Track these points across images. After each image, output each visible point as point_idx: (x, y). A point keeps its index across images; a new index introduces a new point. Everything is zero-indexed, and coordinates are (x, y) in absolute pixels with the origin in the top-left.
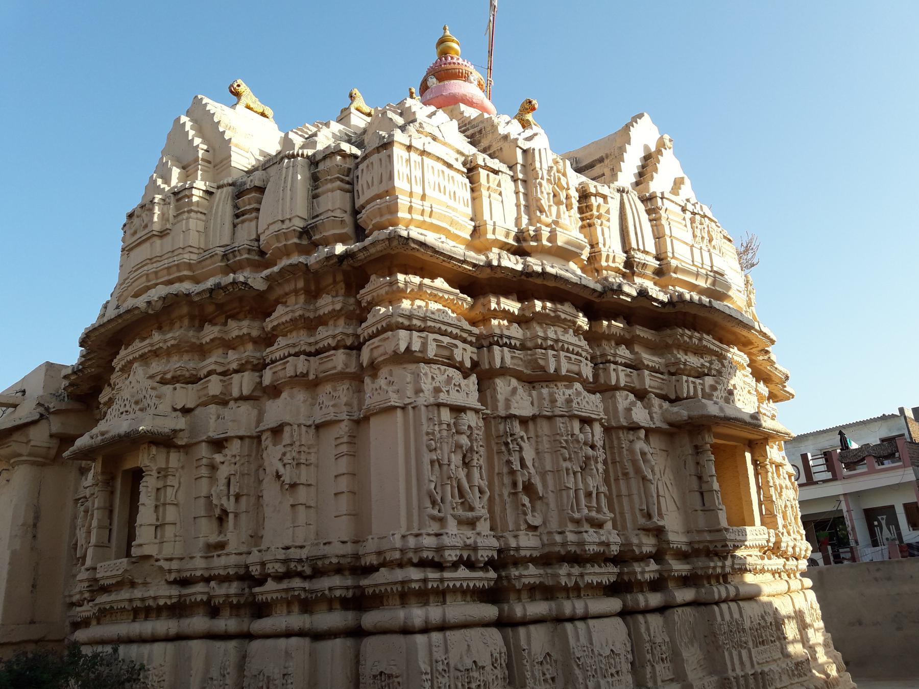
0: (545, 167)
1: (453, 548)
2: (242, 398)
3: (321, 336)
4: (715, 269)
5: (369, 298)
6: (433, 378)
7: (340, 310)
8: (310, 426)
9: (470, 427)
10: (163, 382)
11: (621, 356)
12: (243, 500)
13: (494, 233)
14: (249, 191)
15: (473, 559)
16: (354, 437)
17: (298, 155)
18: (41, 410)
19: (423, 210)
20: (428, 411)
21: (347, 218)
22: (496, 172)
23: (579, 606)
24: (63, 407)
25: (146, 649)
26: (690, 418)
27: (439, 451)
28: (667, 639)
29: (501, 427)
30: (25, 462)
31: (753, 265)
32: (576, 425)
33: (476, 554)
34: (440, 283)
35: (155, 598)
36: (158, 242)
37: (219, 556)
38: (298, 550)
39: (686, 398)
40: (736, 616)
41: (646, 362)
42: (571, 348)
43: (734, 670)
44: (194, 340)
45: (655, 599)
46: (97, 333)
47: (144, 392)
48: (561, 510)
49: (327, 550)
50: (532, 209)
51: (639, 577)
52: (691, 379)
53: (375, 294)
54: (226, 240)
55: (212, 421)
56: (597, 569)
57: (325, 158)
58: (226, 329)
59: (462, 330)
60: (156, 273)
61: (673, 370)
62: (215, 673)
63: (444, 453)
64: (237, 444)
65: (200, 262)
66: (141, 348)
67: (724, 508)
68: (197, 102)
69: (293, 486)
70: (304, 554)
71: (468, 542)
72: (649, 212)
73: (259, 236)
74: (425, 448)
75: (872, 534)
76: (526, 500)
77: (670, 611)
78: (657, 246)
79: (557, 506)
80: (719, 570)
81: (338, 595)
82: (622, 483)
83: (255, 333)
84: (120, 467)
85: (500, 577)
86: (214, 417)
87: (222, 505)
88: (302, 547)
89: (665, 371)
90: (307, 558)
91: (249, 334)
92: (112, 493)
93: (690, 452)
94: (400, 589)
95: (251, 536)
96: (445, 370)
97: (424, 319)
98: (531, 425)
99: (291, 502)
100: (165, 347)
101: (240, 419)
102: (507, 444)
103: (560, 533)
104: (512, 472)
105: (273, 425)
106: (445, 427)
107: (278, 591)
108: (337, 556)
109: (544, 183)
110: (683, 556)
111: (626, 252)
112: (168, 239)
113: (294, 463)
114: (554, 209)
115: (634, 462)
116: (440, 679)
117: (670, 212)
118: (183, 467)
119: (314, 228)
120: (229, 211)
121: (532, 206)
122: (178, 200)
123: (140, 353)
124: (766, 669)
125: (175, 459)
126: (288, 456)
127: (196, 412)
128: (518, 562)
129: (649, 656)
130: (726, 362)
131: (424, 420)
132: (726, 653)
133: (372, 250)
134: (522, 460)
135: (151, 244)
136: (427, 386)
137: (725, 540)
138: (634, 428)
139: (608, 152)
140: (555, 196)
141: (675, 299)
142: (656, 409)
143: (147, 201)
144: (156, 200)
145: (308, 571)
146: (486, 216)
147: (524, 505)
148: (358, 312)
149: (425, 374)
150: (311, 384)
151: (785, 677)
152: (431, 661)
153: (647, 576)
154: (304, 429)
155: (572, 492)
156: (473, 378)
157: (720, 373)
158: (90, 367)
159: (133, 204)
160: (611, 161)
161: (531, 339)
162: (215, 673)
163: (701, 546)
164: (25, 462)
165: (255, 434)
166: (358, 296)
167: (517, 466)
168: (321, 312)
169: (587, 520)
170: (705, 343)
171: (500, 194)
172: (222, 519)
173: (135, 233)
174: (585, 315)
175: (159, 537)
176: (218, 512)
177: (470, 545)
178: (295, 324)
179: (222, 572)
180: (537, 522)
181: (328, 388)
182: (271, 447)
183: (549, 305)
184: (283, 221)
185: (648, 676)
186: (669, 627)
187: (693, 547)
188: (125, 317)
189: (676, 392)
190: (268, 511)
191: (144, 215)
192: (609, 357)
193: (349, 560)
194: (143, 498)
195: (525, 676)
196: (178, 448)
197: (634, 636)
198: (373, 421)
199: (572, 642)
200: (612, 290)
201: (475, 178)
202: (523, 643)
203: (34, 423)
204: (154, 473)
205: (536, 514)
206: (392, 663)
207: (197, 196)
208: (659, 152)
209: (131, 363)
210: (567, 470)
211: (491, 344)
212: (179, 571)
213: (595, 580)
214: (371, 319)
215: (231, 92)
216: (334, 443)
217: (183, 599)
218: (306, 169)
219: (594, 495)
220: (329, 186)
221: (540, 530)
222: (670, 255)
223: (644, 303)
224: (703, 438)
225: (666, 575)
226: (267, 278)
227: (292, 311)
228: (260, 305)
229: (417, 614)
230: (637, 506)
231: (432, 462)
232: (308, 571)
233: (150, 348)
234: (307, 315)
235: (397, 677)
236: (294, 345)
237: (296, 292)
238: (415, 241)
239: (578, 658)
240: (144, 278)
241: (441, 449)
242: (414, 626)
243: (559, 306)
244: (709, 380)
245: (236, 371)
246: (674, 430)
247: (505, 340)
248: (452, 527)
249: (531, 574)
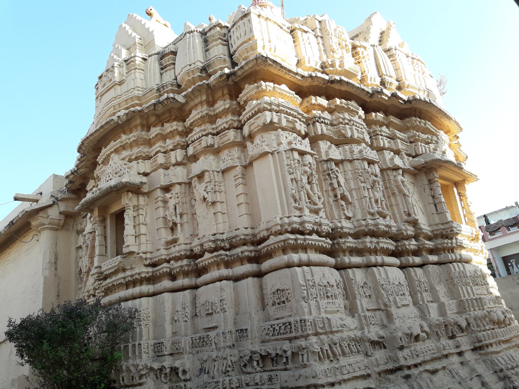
0: (333, 30)
1: (309, 222)
2: (178, 164)
3: (219, 124)
4: (428, 88)
5: (245, 98)
6: (286, 137)
7: (228, 108)
8: (218, 172)
9: (310, 163)
10: (130, 161)
11: (384, 132)
12: (185, 216)
13: (309, 63)
14: (167, 54)
15: (320, 230)
16: (244, 175)
17: (194, 31)
18: (53, 199)
19: (271, 48)
20: (286, 154)
21: (227, 58)
22: (306, 32)
23: (379, 259)
24: (66, 196)
25: (137, 301)
26: (426, 163)
27: (295, 174)
28: (427, 281)
29: (325, 166)
30: (47, 228)
31: (444, 93)
32: (366, 164)
33: (321, 228)
34: (284, 87)
35: (139, 274)
36: (118, 87)
37: (174, 247)
38: (221, 235)
39: (421, 155)
40: (462, 269)
41: (398, 135)
42: (358, 125)
43: (464, 296)
44: (145, 137)
45: (417, 260)
46: (88, 140)
47: (120, 167)
48: (362, 209)
49: (237, 233)
50: (328, 51)
51: (408, 247)
52: (423, 144)
53: (248, 95)
54: (158, 81)
55: (162, 177)
56: (385, 240)
57: (210, 29)
58: (163, 128)
59: (299, 114)
60: (119, 104)
61: (412, 140)
62: (179, 308)
63: (298, 175)
64: (178, 187)
65: (144, 95)
66: (115, 145)
67: (449, 211)
68: (130, 17)
69: (214, 203)
70: (224, 237)
71: (317, 220)
72: (390, 57)
73: (176, 77)
74: (287, 173)
75: (508, 270)
76: (343, 203)
77: (426, 266)
78: (397, 74)
79: (360, 207)
80: (450, 245)
81: (247, 255)
82: (392, 199)
83: (180, 129)
84: (110, 208)
85: (333, 244)
86: (163, 175)
87: (173, 220)
88: (222, 234)
89: (408, 141)
90: (226, 239)
91: (177, 129)
92: (105, 227)
93: (427, 183)
94: (283, 244)
95: (191, 235)
96: (292, 134)
97: (278, 105)
98: (340, 165)
99: (214, 211)
100: (129, 142)
101: (178, 174)
102: (329, 175)
103: (364, 220)
104: (334, 189)
105: (198, 172)
106: (296, 161)
107: (212, 257)
108: (244, 235)
109: (333, 37)
110: (430, 239)
111: (380, 77)
112: (124, 85)
113: (213, 191)
114: (340, 51)
115: (398, 187)
116: (311, 290)
117: (400, 58)
118: (147, 205)
119: (209, 66)
120: (157, 67)
121: (327, 50)
122: (127, 65)
123: (114, 148)
124: (482, 297)
125: (142, 200)
126: (209, 187)
127: (152, 174)
128: (343, 235)
129: (418, 288)
130: (439, 137)
131: (285, 158)
132: (459, 288)
133: (246, 68)
134: (338, 182)
135: (115, 90)
136: (284, 141)
137: (452, 227)
138: (396, 169)
139: (361, 31)
140: (339, 44)
141: (411, 98)
142: (406, 160)
143: (110, 67)
144: (115, 65)
145: (228, 246)
146: (304, 54)
147: (342, 206)
148: (238, 109)
149: (282, 135)
150: (216, 151)
151: (491, 303)
152: (305, 280)
153: (412, 247)
154: (216, 173)
155: (368, 199)
156: (307, 140)
157: (437, 142)
158: (82, 167)
159: (102, 70)
160: (363, 35)
161: (336, 120)
162: (179, 308)
163: (438, 232)
164: (47, 228)
165: (187, 181)
166: (238, 99)
167: (336, 185)
168: (218, 111)
169: (377, 213)
170: (427, 126)
171: (309, 43)
172: (173, 228)
173: (104, 85)
174: (363, 110)
175: (137, 242)
176: (171, 224)
177: (317, 223)
178: (203, 120)
179: (177, 254)
180: (350, 215)
181: (226, 152)
182: (198, 185)
183: (343, 101)
184: (190, 65)
185: (420, 299)
186: (427, 274)
187: (434, 234)
188: (105, 128)
189: (415, 152)
190: (199, 220)
191: (109, 75)
192: (378, 132)
193: (250, 237)
194: (126, 221)
195: (355, 294)
196: (143, 194)
197: (409, 279)
198: (255, 164)
199: (378, 277)
200: (378, 92)
201: (295, 35)
202: (351, 276)
203: (50, 206)
204: (131, 208)
205: (349, 211)
206: (284, 283)
207: (138, 60)
208: (389, 29)
209: (109, 156)
210: (364, 187)
211: (314, 122)
212: (151, 259)
213: (385, 246)
214: (248, 108)
215: (147, 13)
216: (233, 179)
217: (155, 274)
218: (200, 38)
219: (379, 201)
220: (215, 43)
221: (352, 219)
222: (404, 78)
223: (394, 101)
224: (433, 175)
225: (421, 247)
226: (185, 96)
227: (202, 112)
228: (180, 113)
229: (295, 257)
230: (402, 210)
231: (292, 180)
232: (228, 246)
233: (120, 144)
234: (210, 113)
235: (287, 290)
236: (204, 130)
237: (201, 103)
238: (270, 59)
239: (382, 285)
240: (112, 108)
241: (296, 173)
242: (293, 262)
243: (349, 102)
244: (432, 146)
245: (172, 150)
246: (416, 171)
247: (322, 120)
248: (307, 212)
249: (350, 242)
